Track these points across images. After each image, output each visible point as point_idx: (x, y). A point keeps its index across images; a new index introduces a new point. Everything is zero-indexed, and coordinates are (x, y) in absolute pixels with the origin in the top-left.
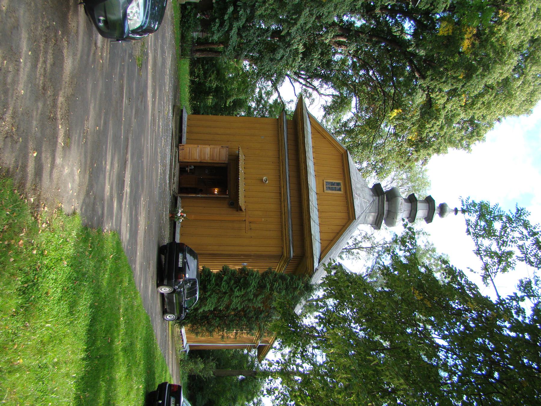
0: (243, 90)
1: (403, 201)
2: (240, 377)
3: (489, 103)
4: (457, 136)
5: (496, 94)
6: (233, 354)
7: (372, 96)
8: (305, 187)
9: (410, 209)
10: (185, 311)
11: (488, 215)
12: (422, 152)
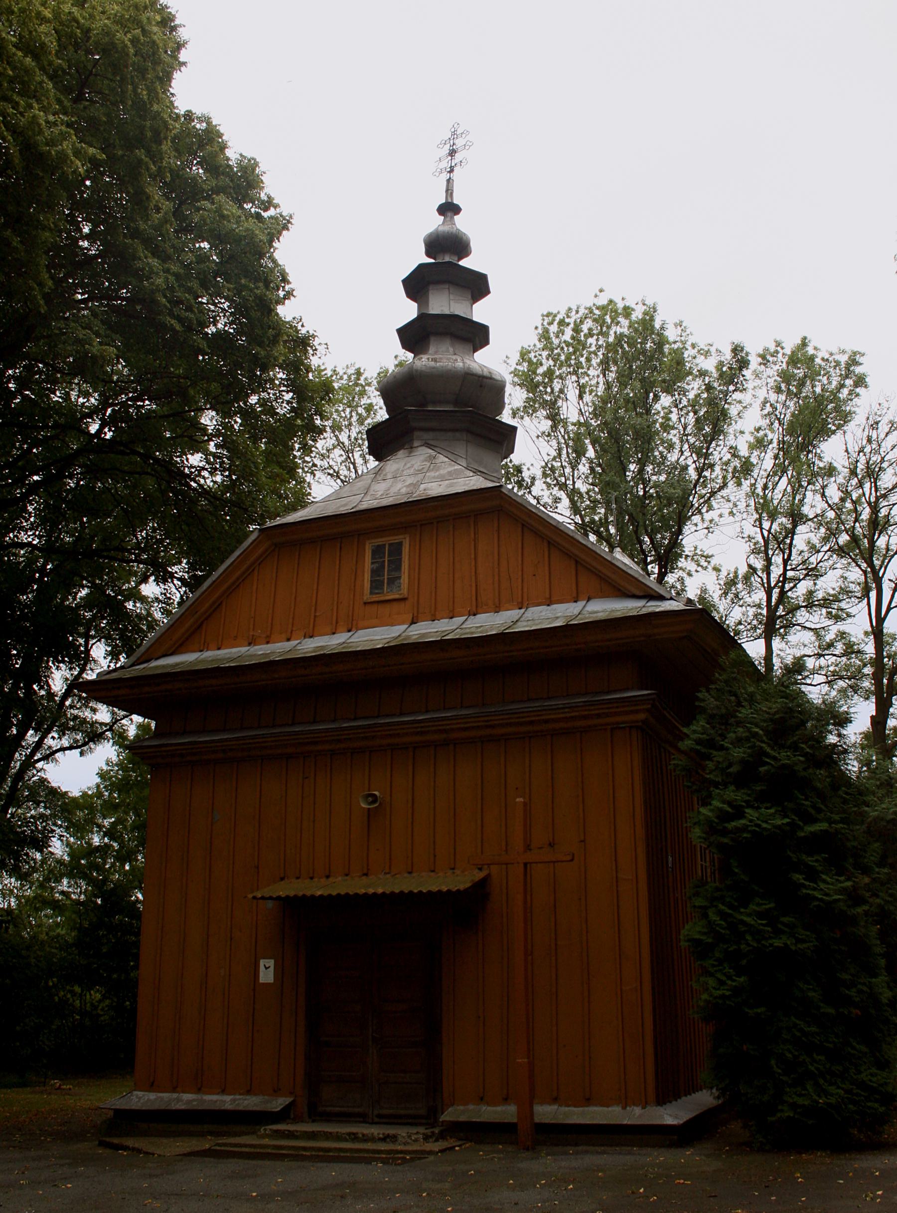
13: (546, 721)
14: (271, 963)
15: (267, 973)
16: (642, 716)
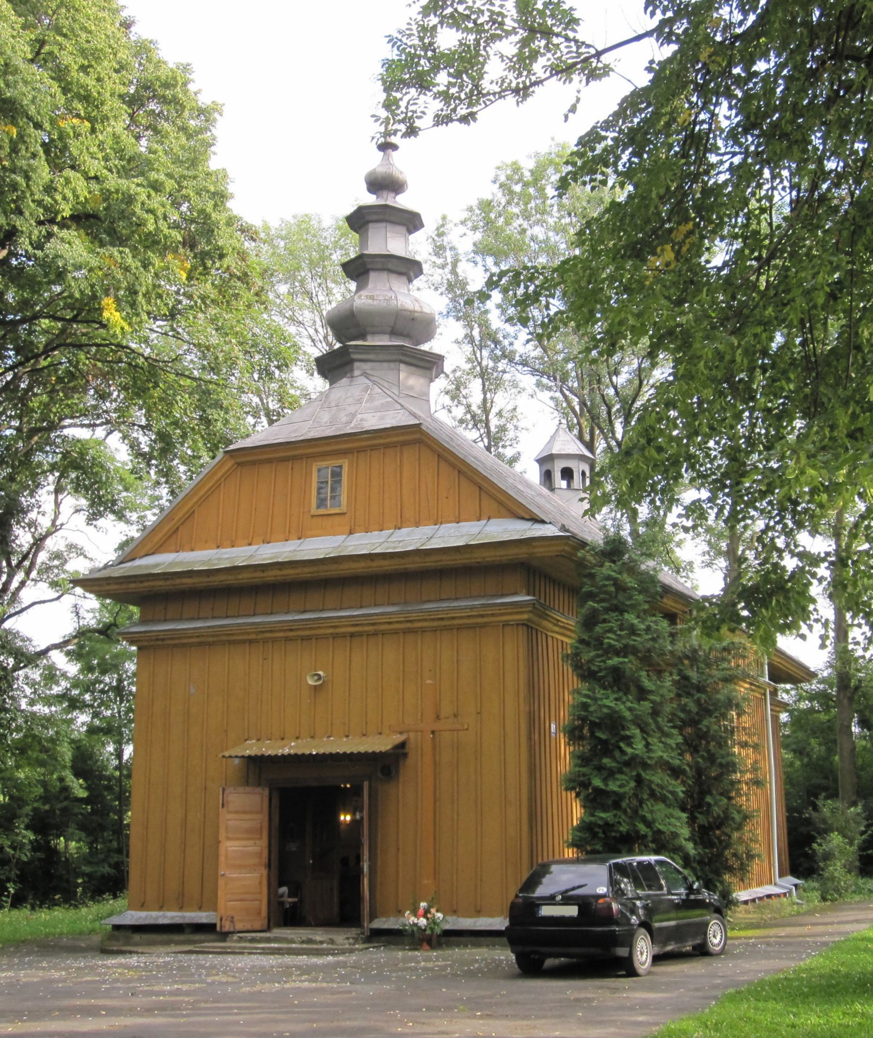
0: (45, 750)
1: (364, 293)
2: (855, 729)
3: (83, 52)
4: (177, 141)
5: (58, 30)
6: (795, 751)
7: (60, 380)
8: (334, 567)
9: (384, 275)
10: (698, 891)
11: (418, 64)
12: (224, 239)
13: (453, 618)
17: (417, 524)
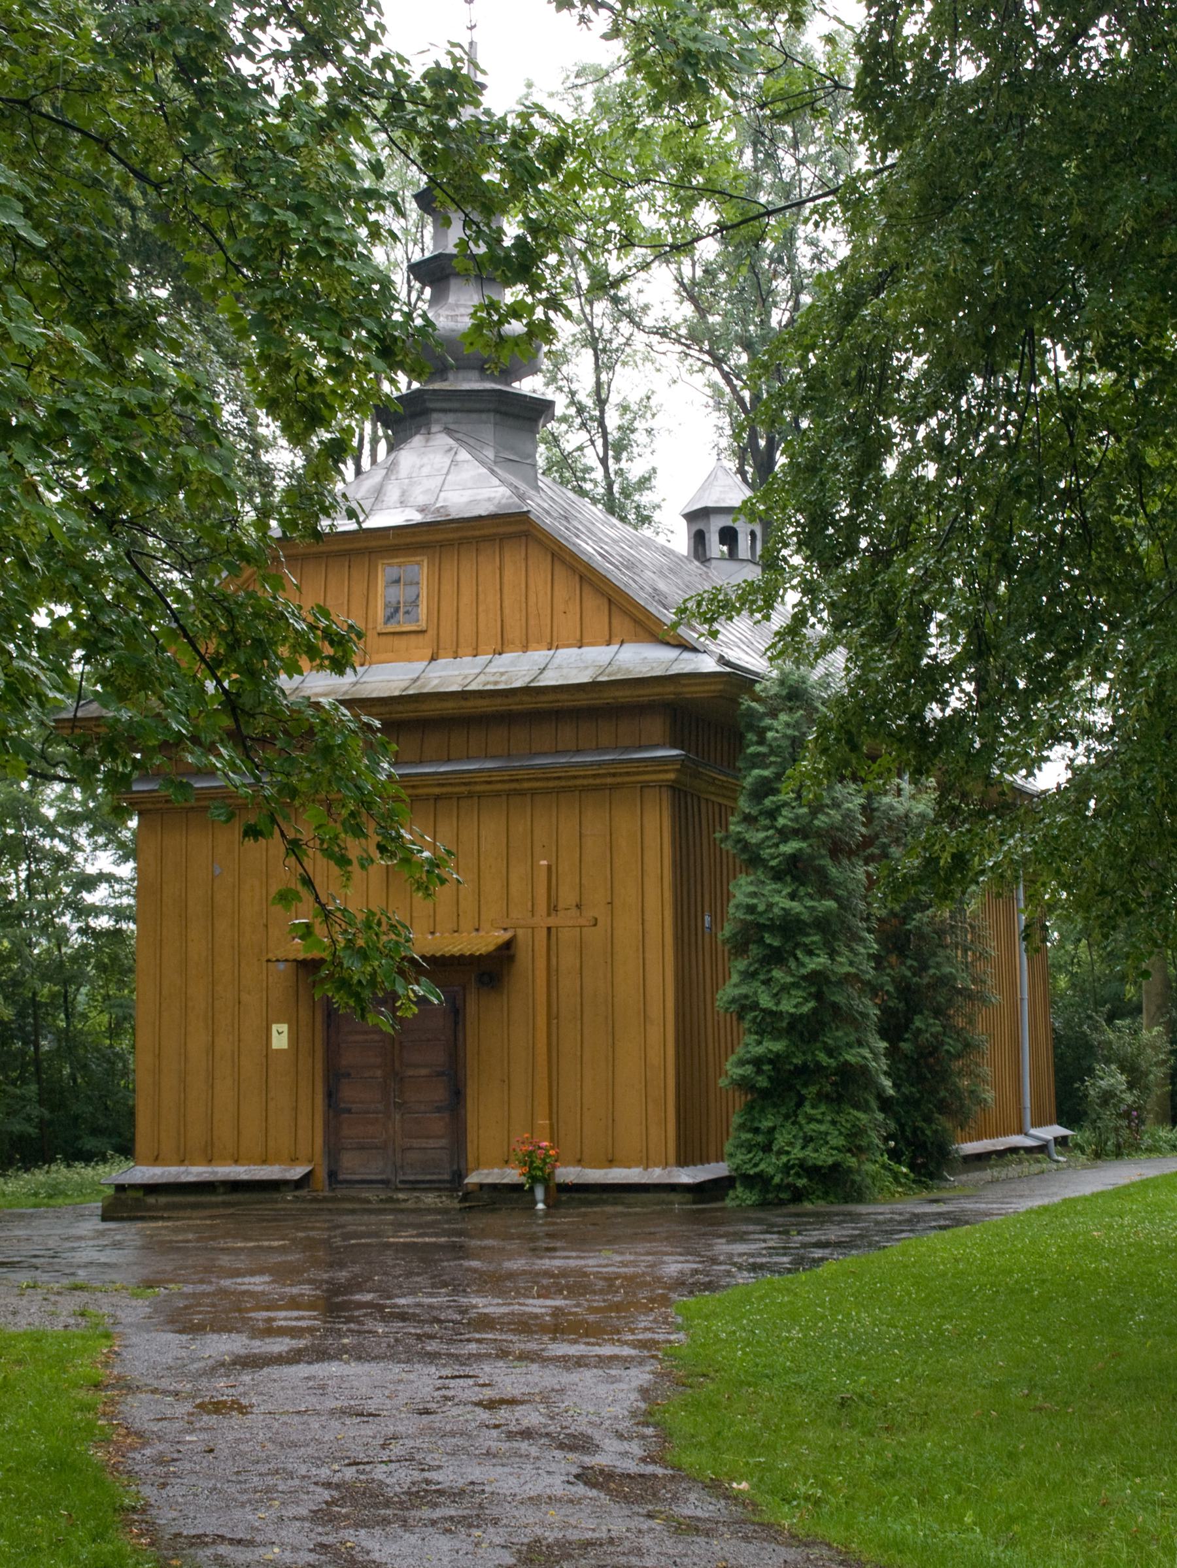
13: (575, 777)
14: (284, 1028)
15: (280, 1037)
16: (672, 776)
17: (525, 648)
